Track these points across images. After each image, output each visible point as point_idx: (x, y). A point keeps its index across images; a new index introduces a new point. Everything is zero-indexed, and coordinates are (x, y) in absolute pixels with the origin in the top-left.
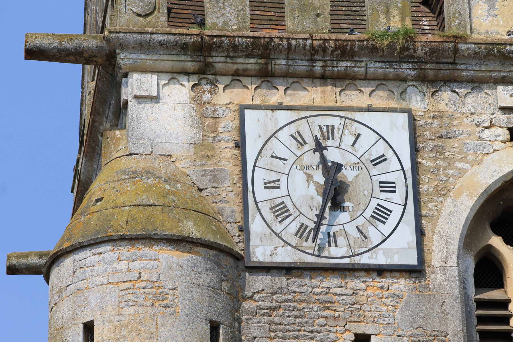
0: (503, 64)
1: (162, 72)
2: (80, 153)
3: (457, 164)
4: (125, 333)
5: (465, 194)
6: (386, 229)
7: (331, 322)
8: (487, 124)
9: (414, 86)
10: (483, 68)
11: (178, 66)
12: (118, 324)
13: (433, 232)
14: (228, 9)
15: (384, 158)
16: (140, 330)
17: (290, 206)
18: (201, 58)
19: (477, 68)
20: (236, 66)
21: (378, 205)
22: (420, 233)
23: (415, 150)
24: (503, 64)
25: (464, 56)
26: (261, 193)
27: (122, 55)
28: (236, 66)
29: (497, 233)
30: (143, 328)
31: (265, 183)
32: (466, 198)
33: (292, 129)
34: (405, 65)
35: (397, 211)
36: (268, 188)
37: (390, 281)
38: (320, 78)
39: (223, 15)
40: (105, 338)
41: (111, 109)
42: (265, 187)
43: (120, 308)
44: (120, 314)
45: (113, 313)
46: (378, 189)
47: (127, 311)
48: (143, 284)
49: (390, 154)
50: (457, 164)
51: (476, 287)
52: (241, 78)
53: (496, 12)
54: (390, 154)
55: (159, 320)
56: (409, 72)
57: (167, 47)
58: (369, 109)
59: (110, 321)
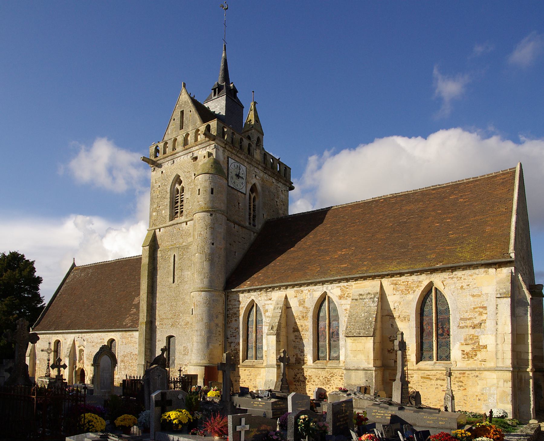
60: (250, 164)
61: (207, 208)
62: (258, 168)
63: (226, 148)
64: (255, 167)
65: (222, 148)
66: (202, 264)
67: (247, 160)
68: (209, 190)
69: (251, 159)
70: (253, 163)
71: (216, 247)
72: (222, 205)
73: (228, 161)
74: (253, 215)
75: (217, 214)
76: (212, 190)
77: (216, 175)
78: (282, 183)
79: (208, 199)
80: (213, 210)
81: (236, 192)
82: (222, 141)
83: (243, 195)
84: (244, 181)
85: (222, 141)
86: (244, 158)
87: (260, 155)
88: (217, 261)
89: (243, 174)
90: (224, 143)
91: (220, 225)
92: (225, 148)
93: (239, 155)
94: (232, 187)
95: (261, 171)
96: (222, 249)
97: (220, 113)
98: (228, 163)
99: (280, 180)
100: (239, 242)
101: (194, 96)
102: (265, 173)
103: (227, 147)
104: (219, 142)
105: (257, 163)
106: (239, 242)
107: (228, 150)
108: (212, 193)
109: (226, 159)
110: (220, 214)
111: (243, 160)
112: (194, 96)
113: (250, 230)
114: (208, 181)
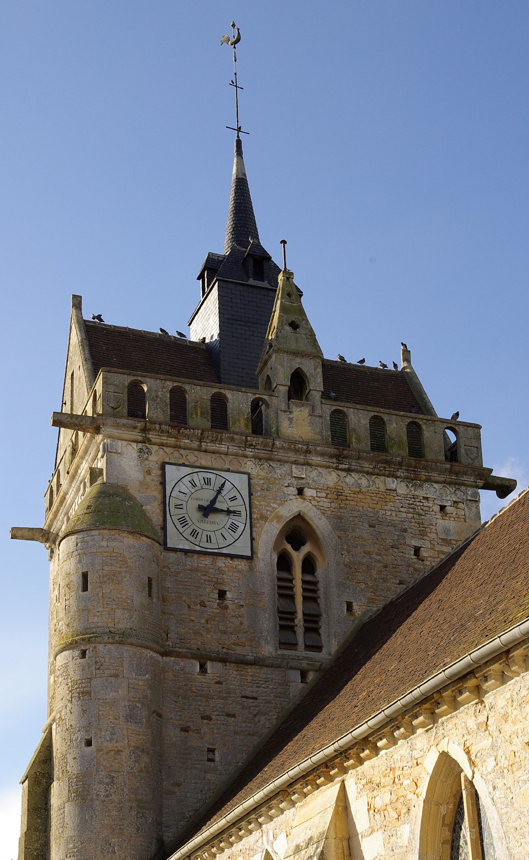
0: (296, 454)
1: (123, 440)
2: (492, 519)
3: (272, 504)
4: (105, 579)
5: (275, 521)
6: (236, 536)
7: (207, 583)
8: (287, 485)
9: (251, 460)
10: (286, 455)
11: (133, 437)
12: (101, 574)
13: (259, 539)
14: (159, 409)
15: (195, 530)
16: (113, 579)
17: (188, 519)
18: (144, 435)
19: (283, 455)
20: (162, 441)
21: (232, 522)
22: (252, 539)
23: (250, 494)
24: (296, 454)
25: (276, 447)
26: (173, 511)
27: (103, 429)
28: (162, 441)
29: (289, 542)
30: (115, 578)
31: (175, 506)
32: (276, 523)
33: (188, 478)
34: (247, 449)
35: (241, 527)
36: (177, 508)
37: (237, 563)
38: (204, 452)
39: (156, 412)
40: (94, 581)
41: (91, 457)
42: (175, 508)
43: (103, 566)
44: (103, 570)
45: (99, 568)
46: (228, 527)
47: (106, 568)
48: (115, 555)
49: (238, 496)
50: (272, 504)
51: (278, 570)
52: (163, 448)
53: (293, 426)
54: (238, 496)
55: (123, 574)
56: (249, 453)
57: (127, 427)
58: (228, 470)
59: (97, 572)
60: (268, 459)
61: (78, 635)
62: (307, 464)
63: (149, 441)
64: (296, 463)
65: (134, 445)
66: (62, 811)
67: (249, 452)
68: (77, 580)
69: (266, 445)
70: (280, 455)
71: (98, 750)
72: (119, 613)
73: (163, 475)
74: (304, 614)
75: (100, 647)
76: (85, 576)
77: (94, 533)
78: (436, 482)
79: (74, 609)
80: (83, 639)
81: (208, 561)
82: (124, 425)
83: (242, 565)
84: (241, 522)
85: (124, 425)
86: (233, 449)
87: (311, 423)
88: (102, 794)
89: (233, 499)
90: (135, 428)
91: (113, 679)
92: (146, 441)
93: (212, 447)
94: (186, 552)
95: (327, 467)
96: (125, 753)
97: (363, 361)
98: (163, 483)
99: (423, 475)
100: (228, 715)
101: (407, 355)
102: (349, 471)
103: (152, 436)
104: (116, 432)
105: (297, 451)
106: (228, 715)
107: (162, 445)
108: (85, 588)
109: (156, 472)
110: (109, 646)
111: (236, 455)
112: (407, 355)
113: (279, 667)
114: (76, 553)
